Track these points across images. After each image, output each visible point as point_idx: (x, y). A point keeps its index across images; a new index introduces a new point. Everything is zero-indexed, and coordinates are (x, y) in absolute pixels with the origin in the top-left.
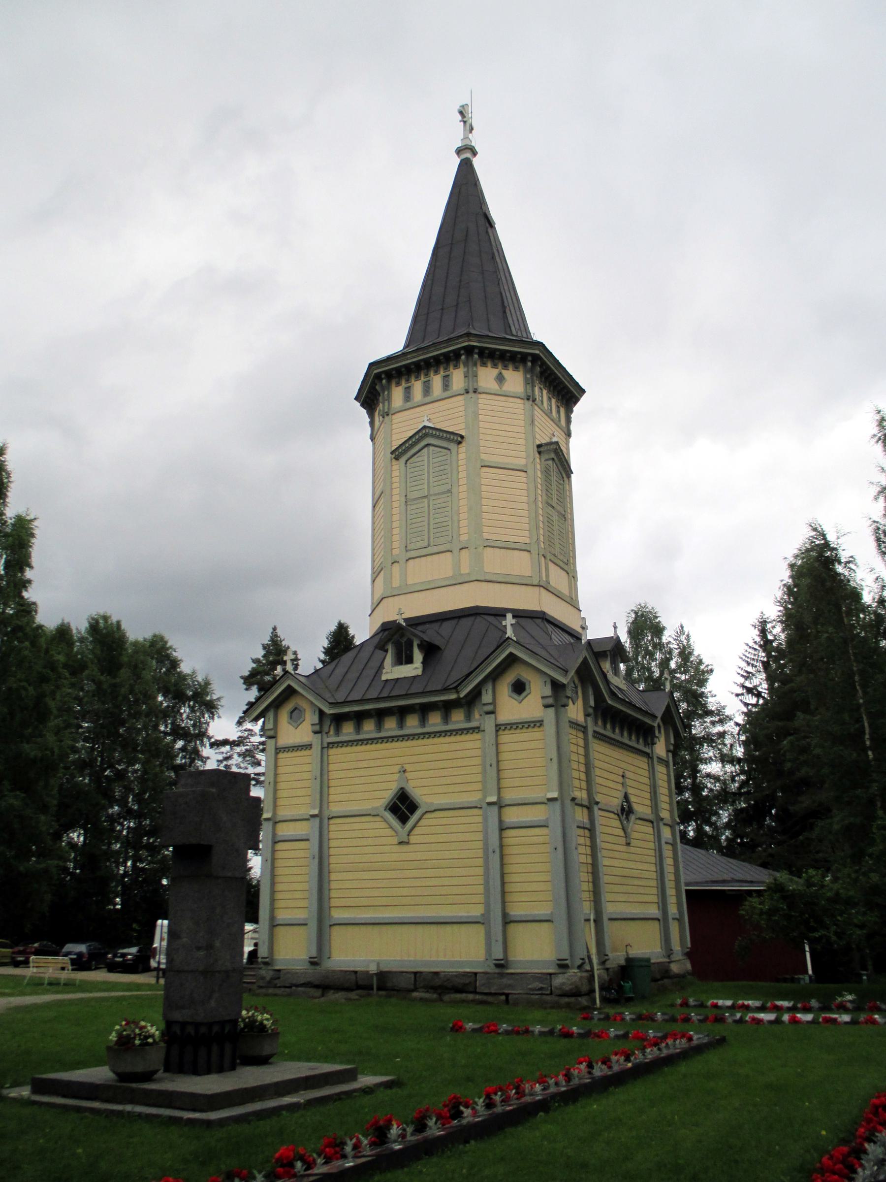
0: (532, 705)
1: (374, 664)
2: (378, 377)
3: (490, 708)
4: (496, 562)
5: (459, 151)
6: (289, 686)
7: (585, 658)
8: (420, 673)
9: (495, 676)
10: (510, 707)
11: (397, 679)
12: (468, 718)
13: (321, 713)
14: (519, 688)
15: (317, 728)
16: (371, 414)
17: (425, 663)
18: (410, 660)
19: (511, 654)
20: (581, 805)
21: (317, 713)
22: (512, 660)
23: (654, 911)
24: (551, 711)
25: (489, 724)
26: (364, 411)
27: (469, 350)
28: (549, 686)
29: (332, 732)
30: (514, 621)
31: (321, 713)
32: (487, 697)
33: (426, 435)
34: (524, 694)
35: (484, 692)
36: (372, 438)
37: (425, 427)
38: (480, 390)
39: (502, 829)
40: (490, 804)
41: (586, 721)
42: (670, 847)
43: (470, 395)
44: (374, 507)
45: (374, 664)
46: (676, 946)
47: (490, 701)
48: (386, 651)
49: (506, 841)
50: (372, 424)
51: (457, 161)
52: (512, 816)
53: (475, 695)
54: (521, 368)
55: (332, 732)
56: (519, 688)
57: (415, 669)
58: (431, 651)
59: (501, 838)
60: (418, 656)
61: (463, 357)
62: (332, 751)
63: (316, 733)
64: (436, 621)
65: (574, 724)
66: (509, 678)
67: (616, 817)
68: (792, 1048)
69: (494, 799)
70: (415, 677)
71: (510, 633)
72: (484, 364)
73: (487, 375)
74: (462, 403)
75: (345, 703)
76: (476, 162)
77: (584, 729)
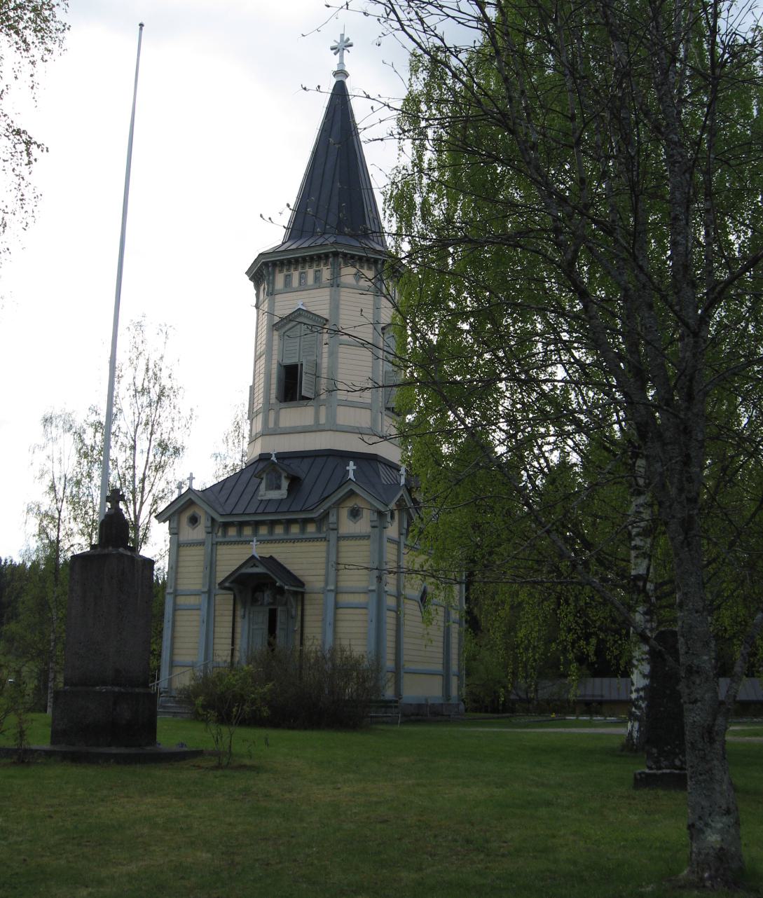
0: (363, 525)
1: (251, 489)
2: (266, 264)
3: (335, 526)
4: (346, 417)
5: (336, 74)
6: (190, 499)
7: (402, 495)
8: (285, 497)
9: (338, 504)
10: (348, 526)
11: (270, 500)
12: (319, 530)
13: (213, 520)
14: (355, 513)
15: (210, 530)
16: (257, 287)
17: (290, 490)
18: (279, 487)
19: (190, 499)
20: (391, 595)
21: (210, 519)
22: (352, 493)
23: (439, 667)
24: (376, 530)
25: (333, 536)
26: (252, 284)
27: (336, 254)
28: (376, 514)
29: (220, 534)
30: (355, 468)
31: (213, 520)
32: (332, 519)
33: (300, 315)
34: (357, 518)
35: (330, 515)
36: (257, 307)
37: (299, 309)
38: (342, 285)
39: (337, 606)
40: (329, 591)
41: (399, 537)
42: (393, 614)
43: (333, 288)
44: (255, 362)
45: (251, 489)
46: (454, 692)
47: (335, 521)
48: (262, 479)
49: (340, 617)
50: (258, 295)
51: (334, 81)
52: (344, 599)
53: (326, 515)
54: (373, 268)
55: (220, 534)
56: (355, 513)
57: (282, 493)
58: (295, 482)
59: (335, 614)
60: (285, 484)
61: (331, 259)
62: (219, 547)
63: (208, 533)
64: (298, 457)
65: (391, 540)
66: (351, 503)
67: (416, 604)
68: (566, 786)
69: (332, 587)
70: (282, 500)
71: (351, 476)
72: (346, 265)
73: (348, 273)
74: (328, 293)
75: (230, 514)
76: (348, 82)
77: (398, 543)
